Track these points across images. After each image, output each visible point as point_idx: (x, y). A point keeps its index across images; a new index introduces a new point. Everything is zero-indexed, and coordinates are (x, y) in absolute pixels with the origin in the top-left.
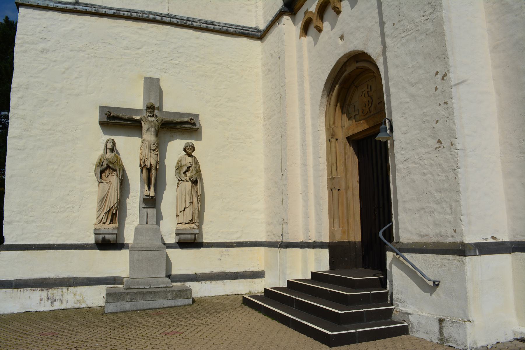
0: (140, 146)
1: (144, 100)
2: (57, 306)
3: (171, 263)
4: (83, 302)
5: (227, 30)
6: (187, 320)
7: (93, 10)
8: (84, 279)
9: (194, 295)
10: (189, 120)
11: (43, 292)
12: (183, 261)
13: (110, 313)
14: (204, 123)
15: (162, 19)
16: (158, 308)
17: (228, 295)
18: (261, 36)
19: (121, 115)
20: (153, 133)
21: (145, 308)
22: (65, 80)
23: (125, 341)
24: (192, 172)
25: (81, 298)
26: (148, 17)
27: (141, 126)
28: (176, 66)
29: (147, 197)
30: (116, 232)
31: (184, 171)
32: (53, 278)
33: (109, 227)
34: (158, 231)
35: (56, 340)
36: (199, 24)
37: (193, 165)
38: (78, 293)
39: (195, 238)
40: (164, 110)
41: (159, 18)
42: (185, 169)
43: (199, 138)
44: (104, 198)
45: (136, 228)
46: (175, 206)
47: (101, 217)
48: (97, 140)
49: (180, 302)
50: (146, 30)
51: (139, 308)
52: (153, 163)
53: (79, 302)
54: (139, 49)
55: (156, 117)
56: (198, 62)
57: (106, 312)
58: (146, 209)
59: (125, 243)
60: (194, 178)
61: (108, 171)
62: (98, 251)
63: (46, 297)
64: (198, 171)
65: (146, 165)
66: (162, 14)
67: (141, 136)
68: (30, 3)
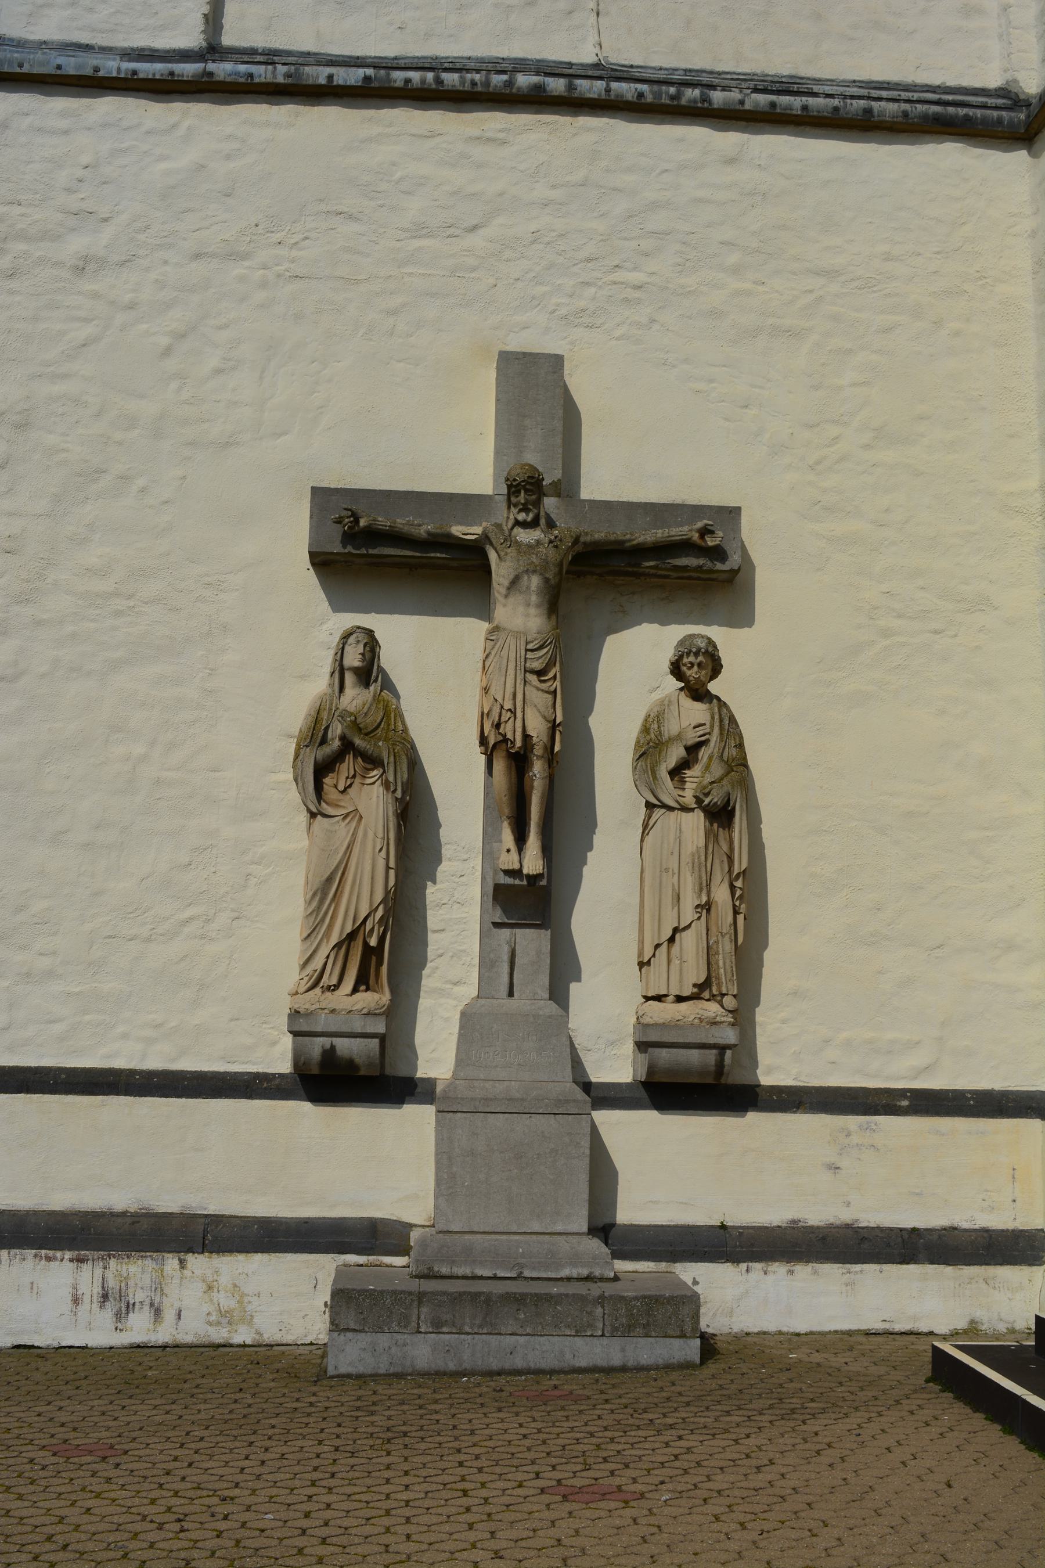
0: (480, 655)
1: (498, 452)
2: (139, 1329)
3: (613, 1174)
4: (242, 1320)
5: (868, 111)
6: (668, 1436)
7: (280, 74)
8: (247, 1222)
9: (711, 1321)
10: (696, 536)
11: (87, 1268)
12: (672, 1169)
13: (349, 1376)
14: (759, 539)
15: (571, 87)
16: (552, 1372)
17: (868, 1333)
18: (1029, 125)
19: (403, 521)
20: (534, 598)
21: (495, 1365)
22: (174, 385)
23: (388, 1512)
24: (707, 768)
25: (232, 1304)
26: (510, 83)
27: (486, 570)
28: (637, 294)
29: (509, 881)
30: (381, 1029)
31: (672, 762)
32: (124, 1214)
33: (353, 1005)
34: (556, 1029)
35: (108, 1480)
36: (735, 95)
37: (714, 738)
38: (224, 1280)
39: (720, 1064)
40: (585, 495)
41: (557, 86)
42: (675, 754)
43: (741, 614)
44: (329, 880)
45: (463, 1014)
46: (632, 918)
47: (317, 963)
48: (302, 633)
49: (648, 1350)
50: (504, 142)
51: (467, 1365)
52: (537, 728)
53: (227, 1317)
54: (474, 228)
55: (551, 524)
56: (736, 270)
57: (331, 1371)
58: (506, 933)
59: (420, 1074)
60: (715, 797)
61: (347, 767)
62: (307, 1106)
63: (97, 1290)
64: (738, 766)
65: (505, 740)
66: (570, 65)
67: (485, 612)
68: (26, 69)
